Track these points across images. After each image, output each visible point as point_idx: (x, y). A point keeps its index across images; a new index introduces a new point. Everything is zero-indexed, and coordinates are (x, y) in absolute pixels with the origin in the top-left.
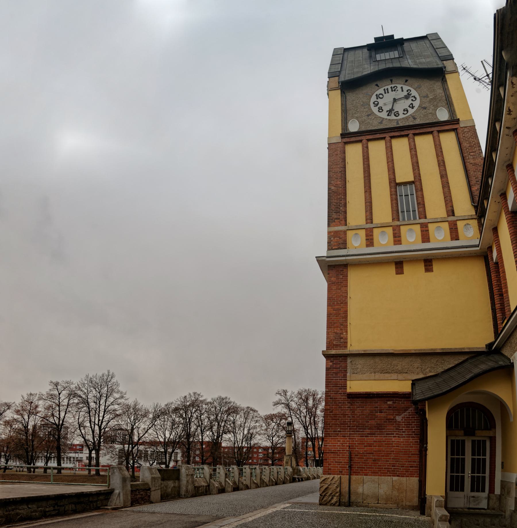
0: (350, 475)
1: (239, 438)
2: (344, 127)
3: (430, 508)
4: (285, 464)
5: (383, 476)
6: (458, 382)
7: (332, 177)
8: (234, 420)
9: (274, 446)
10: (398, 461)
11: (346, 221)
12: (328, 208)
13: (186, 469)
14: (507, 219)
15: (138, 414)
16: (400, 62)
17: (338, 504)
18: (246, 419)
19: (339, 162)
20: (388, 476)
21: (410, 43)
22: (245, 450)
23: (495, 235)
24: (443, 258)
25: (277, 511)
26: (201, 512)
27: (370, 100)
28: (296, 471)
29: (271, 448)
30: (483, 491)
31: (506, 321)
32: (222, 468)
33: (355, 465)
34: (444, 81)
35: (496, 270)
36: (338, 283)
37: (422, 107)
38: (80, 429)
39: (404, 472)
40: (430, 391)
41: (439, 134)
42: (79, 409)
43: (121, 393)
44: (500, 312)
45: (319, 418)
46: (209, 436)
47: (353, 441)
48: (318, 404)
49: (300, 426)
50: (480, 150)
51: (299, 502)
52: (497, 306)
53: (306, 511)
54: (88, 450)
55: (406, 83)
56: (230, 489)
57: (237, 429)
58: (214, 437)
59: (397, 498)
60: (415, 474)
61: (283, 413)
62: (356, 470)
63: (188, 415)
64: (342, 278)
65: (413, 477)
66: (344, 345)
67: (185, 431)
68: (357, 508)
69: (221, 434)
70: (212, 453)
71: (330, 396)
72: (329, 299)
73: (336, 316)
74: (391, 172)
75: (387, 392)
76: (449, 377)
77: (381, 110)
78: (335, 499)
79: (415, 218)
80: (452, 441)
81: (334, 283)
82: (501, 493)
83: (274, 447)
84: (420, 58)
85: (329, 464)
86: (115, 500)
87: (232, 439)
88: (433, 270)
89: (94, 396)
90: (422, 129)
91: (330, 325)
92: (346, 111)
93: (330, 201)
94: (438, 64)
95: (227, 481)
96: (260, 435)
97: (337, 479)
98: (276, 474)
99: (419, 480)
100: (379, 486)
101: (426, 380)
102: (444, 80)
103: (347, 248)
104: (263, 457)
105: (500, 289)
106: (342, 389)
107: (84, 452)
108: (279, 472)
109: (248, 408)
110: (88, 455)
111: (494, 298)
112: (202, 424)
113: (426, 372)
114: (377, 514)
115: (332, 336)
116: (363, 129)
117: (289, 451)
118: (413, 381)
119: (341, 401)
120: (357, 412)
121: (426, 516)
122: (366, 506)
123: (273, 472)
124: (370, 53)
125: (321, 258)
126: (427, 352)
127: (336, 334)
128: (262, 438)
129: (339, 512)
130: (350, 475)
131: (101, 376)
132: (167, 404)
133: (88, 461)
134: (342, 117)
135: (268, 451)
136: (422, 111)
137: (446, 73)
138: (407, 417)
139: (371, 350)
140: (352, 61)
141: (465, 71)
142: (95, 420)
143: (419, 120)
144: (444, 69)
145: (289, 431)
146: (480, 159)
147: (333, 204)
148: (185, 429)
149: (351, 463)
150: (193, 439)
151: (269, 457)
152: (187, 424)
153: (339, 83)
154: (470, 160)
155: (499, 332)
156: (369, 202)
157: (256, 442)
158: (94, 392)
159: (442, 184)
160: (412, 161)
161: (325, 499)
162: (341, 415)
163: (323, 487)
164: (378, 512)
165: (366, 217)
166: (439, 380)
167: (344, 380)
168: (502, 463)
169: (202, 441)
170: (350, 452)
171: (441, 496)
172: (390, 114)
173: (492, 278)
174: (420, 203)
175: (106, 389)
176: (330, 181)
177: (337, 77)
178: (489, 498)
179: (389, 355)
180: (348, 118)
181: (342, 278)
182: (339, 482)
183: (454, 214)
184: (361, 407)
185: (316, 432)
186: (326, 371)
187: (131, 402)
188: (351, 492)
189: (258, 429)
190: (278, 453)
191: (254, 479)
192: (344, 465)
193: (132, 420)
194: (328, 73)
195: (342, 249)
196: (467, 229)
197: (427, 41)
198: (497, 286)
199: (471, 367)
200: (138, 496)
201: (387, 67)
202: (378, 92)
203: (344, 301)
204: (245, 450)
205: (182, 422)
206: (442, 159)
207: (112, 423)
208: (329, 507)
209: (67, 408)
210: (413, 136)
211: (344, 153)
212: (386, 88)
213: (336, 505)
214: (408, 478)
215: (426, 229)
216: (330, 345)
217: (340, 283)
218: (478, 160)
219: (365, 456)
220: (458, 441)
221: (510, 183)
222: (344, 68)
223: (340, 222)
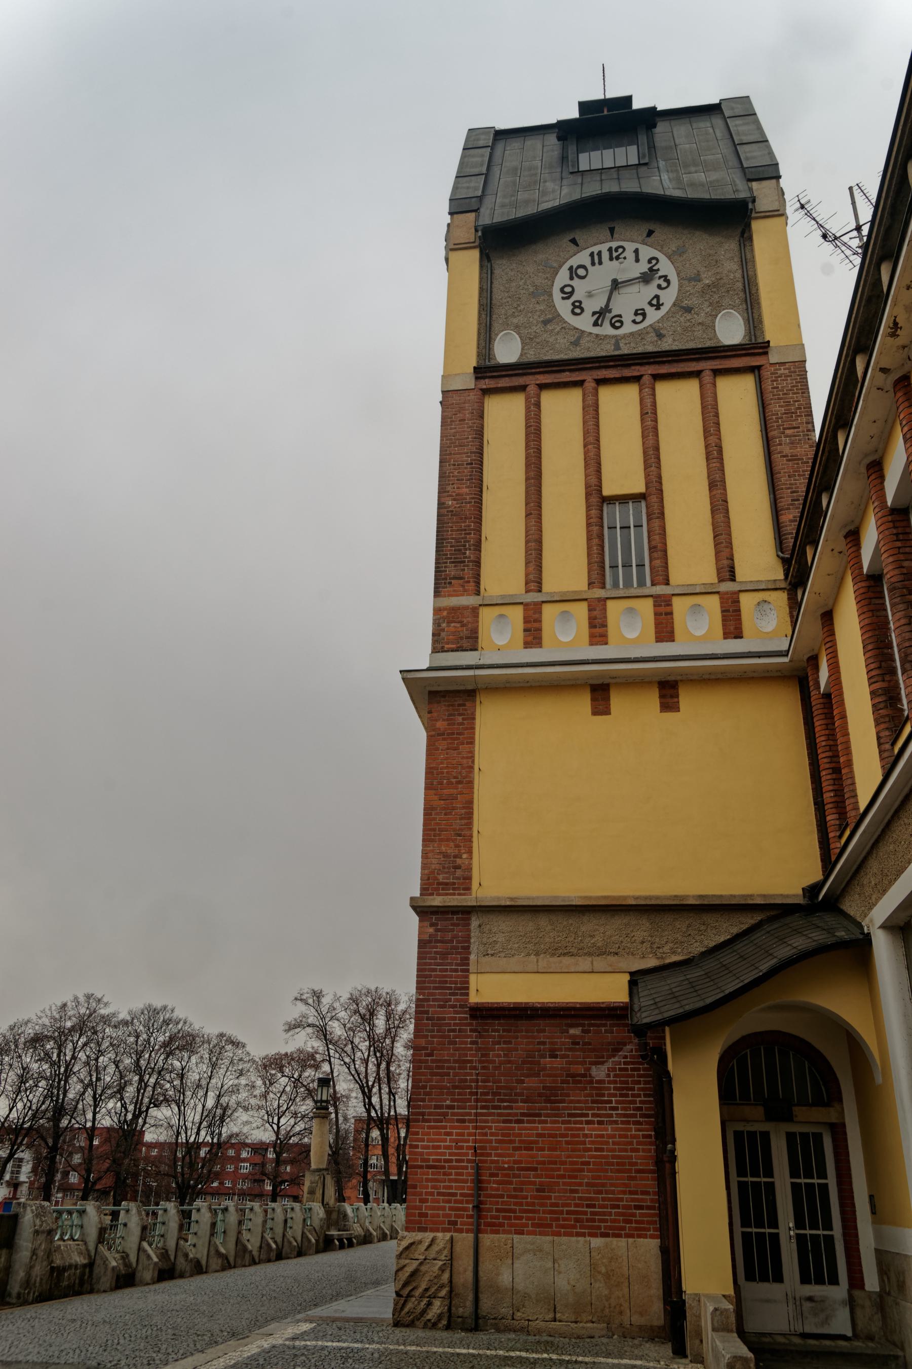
0: (478, 1231)
1: (191, 1119)
2: (484, 351)
3: (699, 1334)
4: (306, 1195)
5: (566, 1234)
6: (742, 978)
7: (449, 476)
8: (183, 1069)
9: (281, 1142)
10: (601, 1192)
11: (478, 583)
12: (437, 551)
13: (37, 1216)
14: (857, 593)
16: (639, 178)
17: (444, 1322)
18: (214, 1066)
19: (468, 438)
20: (578, 1235)
21: (673, 123)
22: (202, 1153)
23: (825, 629)
24: (704, 679)
25: (274, 1347)
26: (56, 1354)
27: (553, 282)
28: (334, 1216)
29: (274, 1145)
30: (834, 1280)
31: (847, 833)
32: (134, 1211)
34: (746, 237)
35: (826, 711)
36: (453, 734)
37: (682, 307)
39: (619, 1221)
40: (674, 1000)
41: (715, 377)
44: (833, 810)
45: (399, 1066)
46: (113, 1114)
47: (486, 1134)
48: (398, 1027)
49: (352, 1086)
50: (808, 423)
51: (337, 1315)
52: (828, 796)
53: (356, 1345)
55: (650, 240)
56: (148, 1275)
57: (189, 1094)
58: (125, 1115)
59: (607, 1304)
60: (649, 1230)
61: (310, 1050)
62: (492, 1217)
63: (65, 1054)
64: (462, 724)
65: (645, 1237)
66: (463, 883)
67: (52, 1100)
68: (497, 1336)
70: (114, 1161)
71: (427, 1012)
72: (430, 772)
73: (445, 814)
74: (592, 469)
75: (567, 1003)
76: (719, 966)
77: (577, 308)
78: (437, 1307)
79: (641, 583)
80: (738, 1135)
81: (444, 734)
82: (880, 1287)
83: (280, 1145)
84: (693, 169)
85: (421, 1201)
87: (175, 1121)
88: (679, 708)
90: (675, 365)
91: (430, 834)
92: (491, 307)
93: (443, 535)
94: (737, 191)
95: (145, 1251)
96: (246, 1109)
97: (441, 1245)
98: (281, 1226)
99: (661, 1247)
100: (556, 1265)
101: (665, 973)
102: (745, 235)
103: (480, 648)
104: (250, 1173)
105: (835, 757)
106: (456, 994)
108: (289, 1220)
109: (222, 1035)
111: (820, 778)
112: (98, 1079)
113: (664, 953)
114: (554, 1357)
115: (435, 862)
116: (531, 357)
117: (318, 1158)
118: (632, 974)
119: (455, 1024)
120: (494, 1055)
121: (691, 1361)
122: (523, 1330)
123: (273, 1219)
124: (564, 149)
125: (413, 673)
126: (664, 903)
127: (444, 856)
128: (251, 1119)
129: (447, 1350)
130: (478, 1231)
132: (15, 1023)
134: (480, 324)
135: (264, 1156)
136: (681, 316)
137: (754, 215)
138: (620, 1069)
139: (528, 898)
140: (515, 169)
141: (803, 212)
143: (670, 341)
144: (750, 206)
145: (322, 1101)
146: (807, 446)
147: (448, 543)
148: (52, 1093)
149: (479, 1196)
150: (70, 1121)
151: (265, 1174)
153: (476, 231)
154: (783, 447)
155: (833, 858)
156: (536, 541)
157: (235, 1130)
159: (711, 504)
160: (643, 443)
161: (409, 1306)
162: (455, 1061)
163: (406, 1269)
164: (555, 1348)
165: (527, 575)
166: (694, 974)
167: (462, 971)
168: (871, 1197)
169: (93, 1127)
170: (477, 1164)
171: (724, 1296)
172: (600, 322)
173: (816, 730)
174: (655, 547)
176: (443, 485)
177: (473, 214)
178: (852, 1303)
179: (572, 911)
180: (496, 326)
181: (462, 724)
182: (449, 1254)
183: (734, 576)
184: (505, 1043)
185: (392, 1103)
186: (419, 947)
188: (482, 1284)
189: (243, 1095)
190: (292, 1162)
191: (218, 1243)
192: (461, 1202)
194: (450, 200)
195: (467, 650)
196: (763, 612)
197: (717, 121)
198: (828, 748)
199: (770, 943)
201: (604, 191)
202: (574, 262)
203: (466, 777)
204: (202, 1153)
205: (48, 1074)
206: (717, 441)
208: (421, 1333)
210: (652, 381)
211: (482, 417)
212: (595, 249)
213: (440, 1325)
214: (631, 1240)
215: (668, 609)
216: (429, 885)
217: (458, 734)
218: (801, 447)
219: (515, 1176)
220: (752, 1134)
221: (871, 508)
222: (492, 188)
223: (463, 586)
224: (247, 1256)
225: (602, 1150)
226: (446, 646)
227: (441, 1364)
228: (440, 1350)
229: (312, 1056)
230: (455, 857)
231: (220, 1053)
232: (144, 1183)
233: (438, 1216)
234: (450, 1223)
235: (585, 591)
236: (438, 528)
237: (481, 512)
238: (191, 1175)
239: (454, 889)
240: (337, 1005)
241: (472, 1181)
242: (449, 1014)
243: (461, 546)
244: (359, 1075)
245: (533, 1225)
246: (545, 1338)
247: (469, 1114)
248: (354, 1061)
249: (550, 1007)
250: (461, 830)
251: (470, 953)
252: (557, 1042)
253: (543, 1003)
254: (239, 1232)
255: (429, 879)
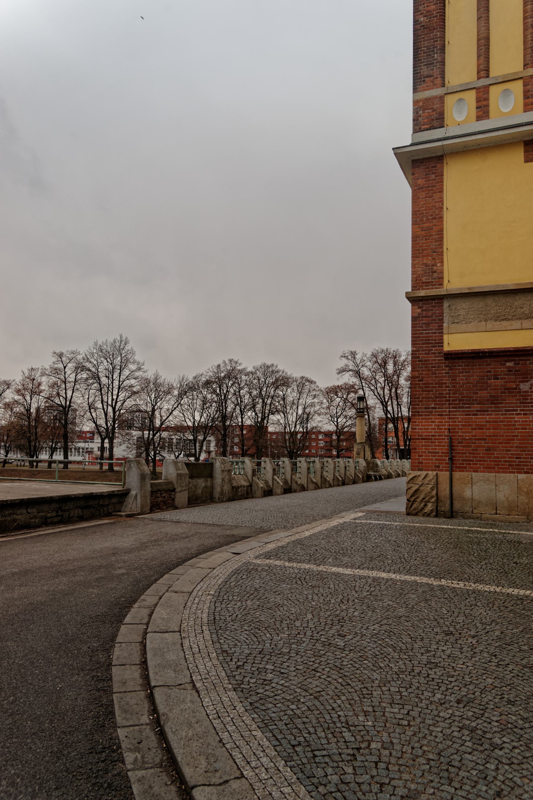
0: (452, 471)
1: (291, 420)
4: (355, 455)
5: (503, 472)
8: (284, 395)
11: (443, 78)
12: (414, 58)
13: (222, 463)
15: (160, 391)
17: (434, 514)
18: (300, 393)
20: (510, 472)
22: (299, 436)
25: (345, 522)
26: (240, 522)
28: (371, 465)
29: (336, 433)
32: (268, 462)
33: (459, 457)
36: (429, 187)
38: (90, 412)
42: (88, 385)
43: (138, 363)
47: (455, 422)
48: (401, 369)
49: (376, 401)
51: (376, 509)
54: (100, 438)
56: (279, 491)
57: (288, 408)
58: (258, 419)
59: (527, 507)
61: (352, 383)
63: (223, 390)
64: (435, 180)
66: (438, 281)
68: (464, 520)
69: (266, 415)
70: (255, 441)
71: (418, 357)
73: (426, 240)
78: (430, 507)
83: (339, 432)
85: (419, 456)
86: (131, 503)
87: (282, 421)
89: (106, 369)
93: (417, 46)
95: (276, 480)
97: (431, 477)
98: (344, 469)
100: (497, 488)
103: (445, 125)
104: (324, 446)
106: (436, 346)
107: (95, 441)
108: (347, 467)
109: (302, 378)
110: (100, 445)
112: (241, 401)
114: (496, 530)
115: (420, 270)
117: (360, 437)
119: (435, 363)
125: (401, 149)
130: (452, 471)
131: (112, 342)
133: (99, 453)
135: (331, 437)
142: (108, 399)
145: (360, 409)
148: (220, 409)
149: (452, 453)
150: (230, 422)
151: (332, 446)
152: (222, 402)
157: (315, 425)
158: (105, 363)
161: (415, 506)
163: (412, 489)
164: (497, 527)
167: (439, 333)
169: (242, 425)
175: (119, 358)
181: (435, 180)
184: (466, 372)
185: (399, 410)
186: (412, 321)
187: (150, 375)
188: (454, 496)
189: (317, 407)
190: (346, 440)
192: (442, 456)
193: (153, 399)
195: (437, 128)
200: (160, 499)
204: (299, 436)
207: (129, 403)
208: (421, 518)
209: (75, 385)
213: (432, 515)
216: (416, 283)
219: (473, 443)
223: (433, 82)
224: (327, 483)
225: (526, 429)
226: (423, 127)
227: (433, 532)
228: (433, 526)
229: (353, 386)
230: (432, 266)
231: (303, 387)
232: (271, 451)
233: (429, 463)
234: (435, 466)
235: (521, 72)
236: (414, 40)
237: (445, 23)
238: (294, 447)
239: (432, 285)
240: (365, 358)
241: (448, 446)
242: (432, 357)
243: (430, 52)
244: (380, 396)
245: (483, 468)
246: (491, 522)
247: (446, 411)
248: (376, 388)
249: (494, 351)
250: (436, 248)
251: (443, 323)
252: (498, 371)
253: (490, 349)
254: (322, 472)
255: (416, 280)
